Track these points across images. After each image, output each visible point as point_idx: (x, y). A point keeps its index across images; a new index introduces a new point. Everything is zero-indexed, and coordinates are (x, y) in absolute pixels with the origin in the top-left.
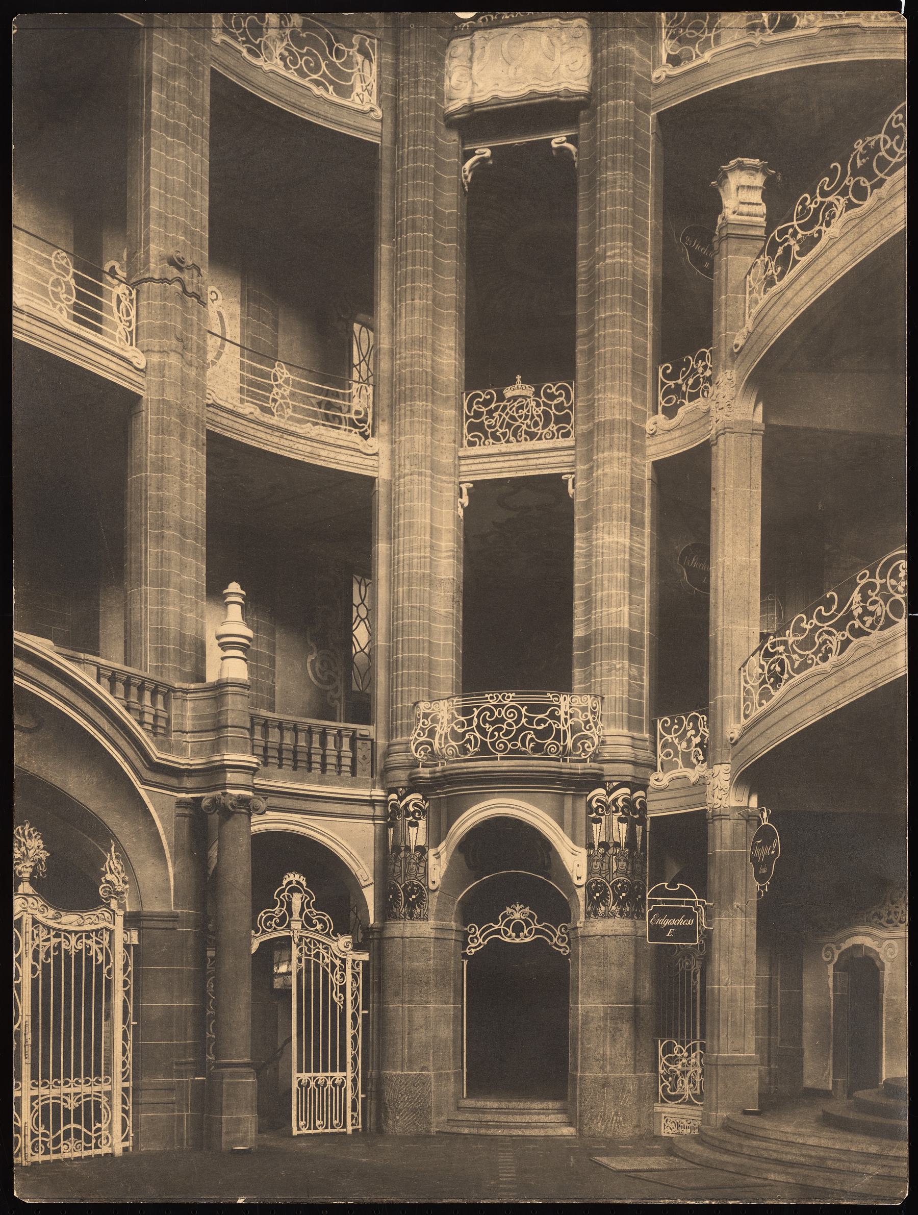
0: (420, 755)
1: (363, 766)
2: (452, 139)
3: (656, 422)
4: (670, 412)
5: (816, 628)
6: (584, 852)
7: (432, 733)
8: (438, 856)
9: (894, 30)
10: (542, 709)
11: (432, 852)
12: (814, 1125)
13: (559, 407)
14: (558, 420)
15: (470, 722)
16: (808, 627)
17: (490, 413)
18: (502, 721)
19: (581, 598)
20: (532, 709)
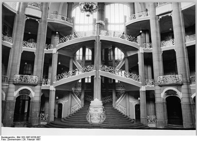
0: (15, 81)
1: (6, 81)
2: (26, 16)
3: (45, 50)
4: (47, 49)
9: (80, 25)
10: (32, 77)
12: (161, 113)
13: (34, 45)
14: (34, 46)
15: (23, 78)
17: (26, 44)
18: (27, 78)
19: (36, 65)
20: (31, 77)
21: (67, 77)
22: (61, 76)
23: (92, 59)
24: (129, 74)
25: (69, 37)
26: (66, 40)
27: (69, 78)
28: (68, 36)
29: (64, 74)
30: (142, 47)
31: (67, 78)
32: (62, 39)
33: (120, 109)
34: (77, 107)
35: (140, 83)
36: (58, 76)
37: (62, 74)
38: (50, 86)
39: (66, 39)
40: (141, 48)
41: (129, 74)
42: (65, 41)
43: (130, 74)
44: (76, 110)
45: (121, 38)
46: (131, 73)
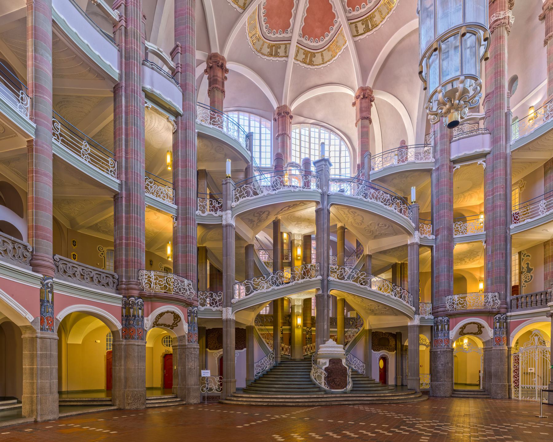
6: (493, 330)
7: (454, 303)
8: (148, 320)
11: (145, 318)
30: (417, 228)
38: (224, 309)
45: (382, 202)
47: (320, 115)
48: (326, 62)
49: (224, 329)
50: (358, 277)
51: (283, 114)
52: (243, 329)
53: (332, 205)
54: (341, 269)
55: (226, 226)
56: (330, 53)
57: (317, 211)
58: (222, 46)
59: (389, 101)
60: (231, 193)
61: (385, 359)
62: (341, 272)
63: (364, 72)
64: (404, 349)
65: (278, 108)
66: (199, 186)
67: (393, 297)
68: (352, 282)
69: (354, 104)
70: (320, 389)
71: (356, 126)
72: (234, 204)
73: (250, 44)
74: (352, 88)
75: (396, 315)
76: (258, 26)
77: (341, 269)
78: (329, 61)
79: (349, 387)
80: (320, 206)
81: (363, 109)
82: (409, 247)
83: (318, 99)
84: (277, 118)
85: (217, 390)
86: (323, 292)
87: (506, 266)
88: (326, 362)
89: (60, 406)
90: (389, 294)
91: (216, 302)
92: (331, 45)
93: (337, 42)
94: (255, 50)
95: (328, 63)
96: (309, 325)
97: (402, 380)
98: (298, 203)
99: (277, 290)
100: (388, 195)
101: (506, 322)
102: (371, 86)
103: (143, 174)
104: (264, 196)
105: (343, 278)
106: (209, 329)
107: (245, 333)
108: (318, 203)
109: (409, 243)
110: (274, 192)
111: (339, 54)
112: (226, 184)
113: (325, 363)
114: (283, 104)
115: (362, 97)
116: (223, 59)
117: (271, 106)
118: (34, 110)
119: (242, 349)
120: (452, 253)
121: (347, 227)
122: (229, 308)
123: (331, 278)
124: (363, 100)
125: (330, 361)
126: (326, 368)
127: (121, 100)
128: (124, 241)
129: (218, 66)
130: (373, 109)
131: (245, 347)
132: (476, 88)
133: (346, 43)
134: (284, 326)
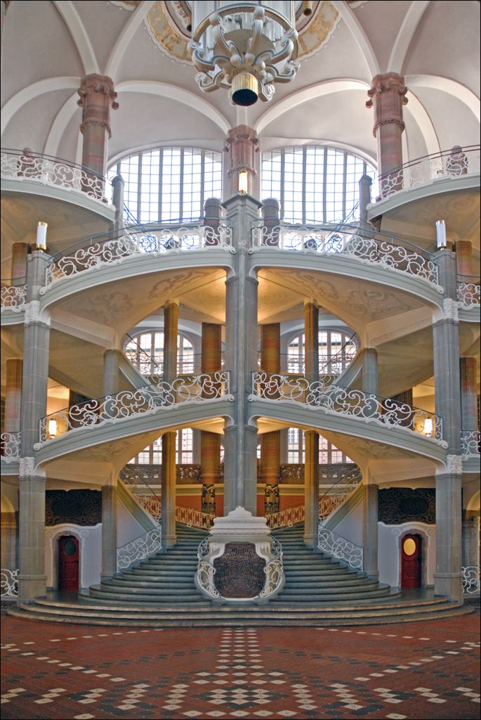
5: (85, 411)
16: (81, 411)
21: (98, 421)
22: (74, 261)
23: (163, 462)
24: (394, 407)
25: (101, 248)
26: (86, 265)
27: (109, 425)
28: (96, 248)
29: (85, 409)
31: (96, 423)
32: (66, 260)
33: (339, 554)
34: (145, 546)
35: (440, 446)
36: (62, 264)
37: (79, 256)
38: (22, 460)
39: (85, 261)
40: (448, 301)
41: (394, 407)
42: (80, 268)
43: (397, 408)
44: (142, 558)
45: (356, 254)
46: (400, 406)
47: (317, 131)
48: (311, 51)
49: (225, 497)
50: (307, 392)
51: (236, 139)
52: (96, 491)
53: (257, 269)
54: (273, 379)
55: (30, 325)
56: (316, 35)
57: (227, 283)
58: (103, 64)
59: (442, 88)
60: (40, 273)
61: (418, 538)
62: (272, 384)
63: (380, 51)
64: (467, 517)
65: (230, 131)
66: (464, 500)
67: (388, 424)
68: (294, 402)
69: (369, 104)
70: (203, 598)
71: (375, 136)
72: (43, 290)
73: (151, 33)
74: (364, 80)
75: (414, 457)
76: (171, 22)
77: (273, 379)
78: (316, 47)
79: (267, 592)
80: (233, 274)
81: (384, 108)
82: (435, 331)
83: (309, 106)
84: (229, 146)
85: (13, 592)
86: (236, 422)
87: (310, 85)
88: (219, 549)
89: (304, 527)
90: (376, 420)
91: (14, 451)
92: (314, 23)
93: (323, 16)
94: (175, 58)
95: (315, 51)
96: (272, 481)
97: (471, 482)
98: (186, 273)
99: (117, 424)
100: (372, 241)
101: (278, 496)
102: (398, 71)
103: (143, 413)
104: (96, 271)
105: (278, 395)
106: (384, 490)
107: (101, 499)
108: (227, 269)
109: (435, 320)
110: (334, 412)
111: (330, 34)
112: (32, 260)
113: (217, 551)
114: (238, 124)
115: (378, 90)
116: (108, 80)
117: (220, 131)
118: (235, 349)
119: (95, 524)
120: (256, 77)
121: (319, 303)
122: (28, 458)
123: (252, 397)
124: (383, 95)
125: (227, 546)
126: (216, 560)
127: (473, 373)
128: (34, 402)
129: (96, 91)
130: (404, 134)
131: (100, 522)
132: (288, 42)
133: (337, 14)
134: (218, 482)
